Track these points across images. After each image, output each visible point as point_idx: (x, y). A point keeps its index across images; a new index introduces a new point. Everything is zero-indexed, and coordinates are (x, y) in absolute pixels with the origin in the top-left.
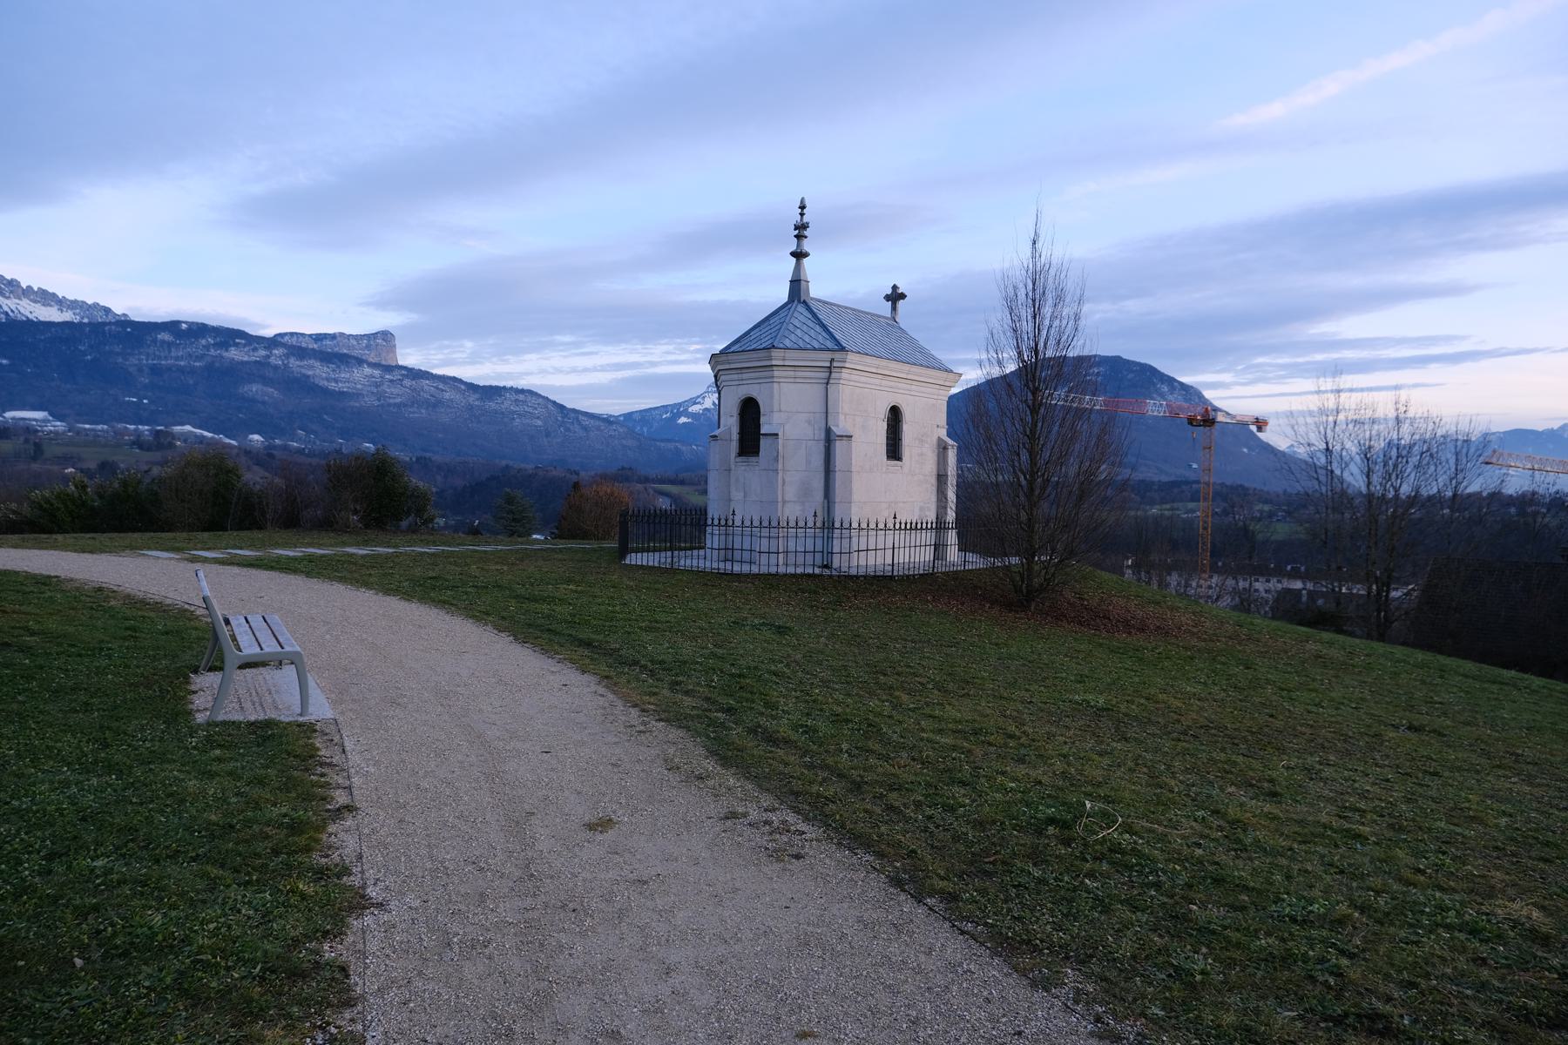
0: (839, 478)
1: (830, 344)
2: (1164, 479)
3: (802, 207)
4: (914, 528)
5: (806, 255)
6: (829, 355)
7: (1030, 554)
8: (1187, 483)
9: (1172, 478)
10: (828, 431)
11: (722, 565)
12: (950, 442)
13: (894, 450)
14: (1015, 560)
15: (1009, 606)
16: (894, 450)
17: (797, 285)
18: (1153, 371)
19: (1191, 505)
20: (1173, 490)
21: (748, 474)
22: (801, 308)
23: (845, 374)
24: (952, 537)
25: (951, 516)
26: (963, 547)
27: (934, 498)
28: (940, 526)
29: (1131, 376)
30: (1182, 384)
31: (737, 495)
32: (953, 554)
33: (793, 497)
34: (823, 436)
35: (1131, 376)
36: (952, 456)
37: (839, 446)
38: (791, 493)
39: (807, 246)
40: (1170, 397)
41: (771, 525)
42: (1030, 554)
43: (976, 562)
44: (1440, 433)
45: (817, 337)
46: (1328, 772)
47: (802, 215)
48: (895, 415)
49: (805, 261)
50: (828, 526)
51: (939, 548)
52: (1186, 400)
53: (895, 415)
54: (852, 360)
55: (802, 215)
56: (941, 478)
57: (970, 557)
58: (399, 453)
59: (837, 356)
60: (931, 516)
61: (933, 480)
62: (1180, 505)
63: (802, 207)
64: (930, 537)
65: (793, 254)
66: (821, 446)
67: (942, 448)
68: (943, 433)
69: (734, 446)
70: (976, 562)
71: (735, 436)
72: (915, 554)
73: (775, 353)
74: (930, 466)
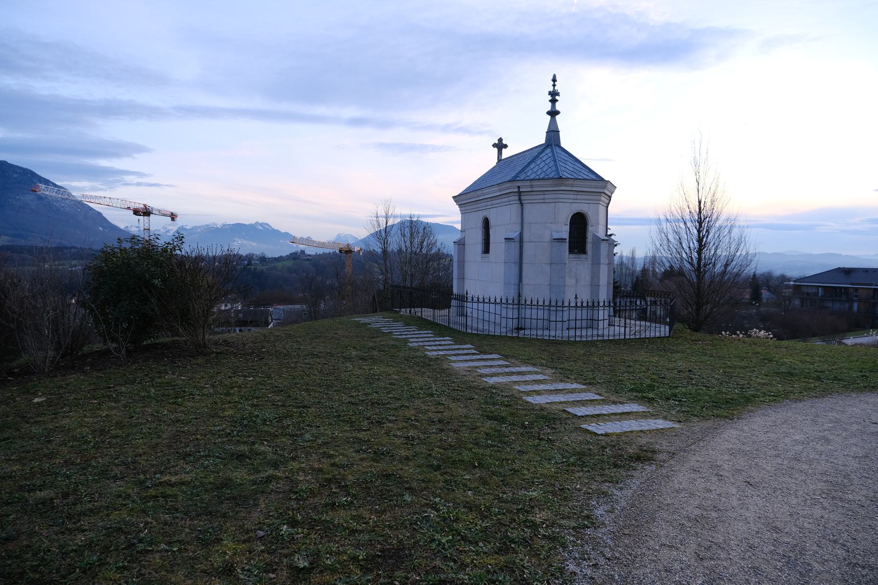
3: (554, 80)
5: (558, 113)
8: (66, 248)
11: (540, 332)
13: (486, 250)
17: (553, 134)
18: (33, 174)
19: (74, 262)
20: (59, 252)
35: (15, 176)
39: (558, 107)
44: (742, 252)
46: (340, 517)
47: (554, 86)
49: (557, 117)
55: (554, 86)
58: (351, 242)
62: (65, 262)
63: (554, 80)
65: (548, 113)
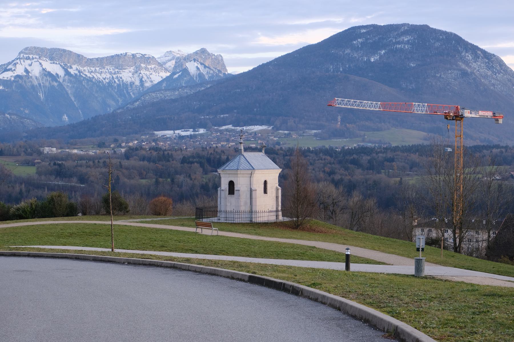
0: (254, 200)
1: (251, 168)
2: (470, 143)
4: (271, 212)
6: (251, 171)
7: (298, 217)
9: (478, 143)
10: (251, 189)
12: (279, 188)
13: (265, 192)
14: (295, 219)
15: (294, 228)
16: (265, 192)
21: (232, 199)
22: (242, 157)
23: (255, 175)
24: (280, 213)
25: (280, 208)
26: (283, 216)
27: (275, 203)
28: (277, 211)
29: (437, 44)
30: (484, 52)
31: (228, 204)
32: (281, 218)
33: (244, 207)
34: (250, 190)
35: (437, 44)
36: (280, 191)
37: (254, 193)
38: (242, 204)
40: (474, 65)
41: (238, 212)
42: (298, 217)
43: (286, 219)
45: (249, 167)
48: (265, 183)
50: (251, 212)
51: (277, 216)
52: (489, 68)
53: (265, 183)
54: (257, 172)
56: (277, 197)
57: (285, 218)
59: (253, 171)
60: (275, 209)
61: (275, 198)
64: (275, 214)
66: (249, 192)
67: (277, 189)
68: (277, 185)
69: (227, 192)
70: (286, 219)
71: (228, 190)
72: (272, 218)
73: (238, 171)
74: (274, 195)
